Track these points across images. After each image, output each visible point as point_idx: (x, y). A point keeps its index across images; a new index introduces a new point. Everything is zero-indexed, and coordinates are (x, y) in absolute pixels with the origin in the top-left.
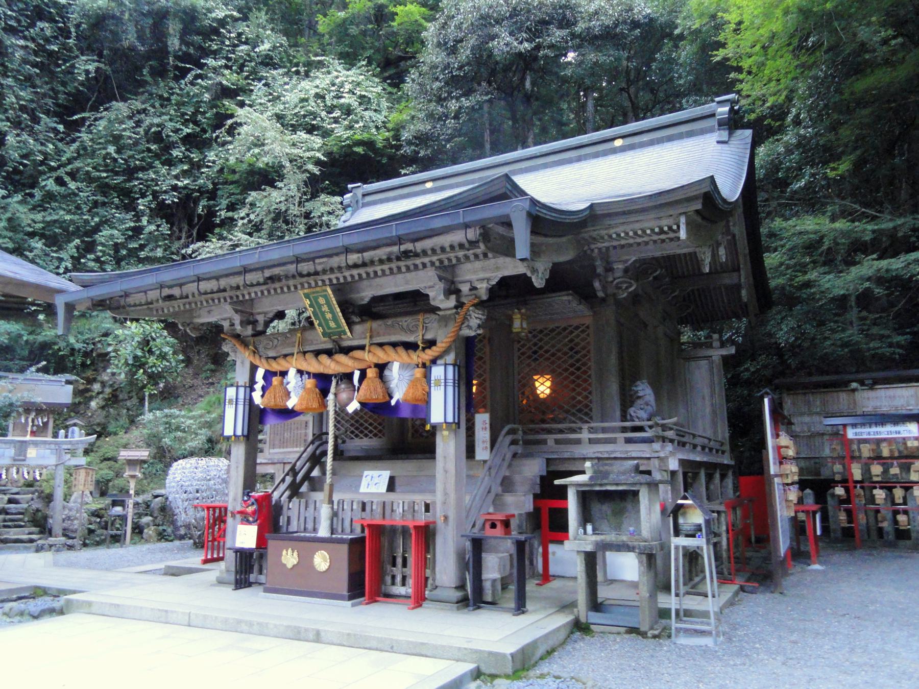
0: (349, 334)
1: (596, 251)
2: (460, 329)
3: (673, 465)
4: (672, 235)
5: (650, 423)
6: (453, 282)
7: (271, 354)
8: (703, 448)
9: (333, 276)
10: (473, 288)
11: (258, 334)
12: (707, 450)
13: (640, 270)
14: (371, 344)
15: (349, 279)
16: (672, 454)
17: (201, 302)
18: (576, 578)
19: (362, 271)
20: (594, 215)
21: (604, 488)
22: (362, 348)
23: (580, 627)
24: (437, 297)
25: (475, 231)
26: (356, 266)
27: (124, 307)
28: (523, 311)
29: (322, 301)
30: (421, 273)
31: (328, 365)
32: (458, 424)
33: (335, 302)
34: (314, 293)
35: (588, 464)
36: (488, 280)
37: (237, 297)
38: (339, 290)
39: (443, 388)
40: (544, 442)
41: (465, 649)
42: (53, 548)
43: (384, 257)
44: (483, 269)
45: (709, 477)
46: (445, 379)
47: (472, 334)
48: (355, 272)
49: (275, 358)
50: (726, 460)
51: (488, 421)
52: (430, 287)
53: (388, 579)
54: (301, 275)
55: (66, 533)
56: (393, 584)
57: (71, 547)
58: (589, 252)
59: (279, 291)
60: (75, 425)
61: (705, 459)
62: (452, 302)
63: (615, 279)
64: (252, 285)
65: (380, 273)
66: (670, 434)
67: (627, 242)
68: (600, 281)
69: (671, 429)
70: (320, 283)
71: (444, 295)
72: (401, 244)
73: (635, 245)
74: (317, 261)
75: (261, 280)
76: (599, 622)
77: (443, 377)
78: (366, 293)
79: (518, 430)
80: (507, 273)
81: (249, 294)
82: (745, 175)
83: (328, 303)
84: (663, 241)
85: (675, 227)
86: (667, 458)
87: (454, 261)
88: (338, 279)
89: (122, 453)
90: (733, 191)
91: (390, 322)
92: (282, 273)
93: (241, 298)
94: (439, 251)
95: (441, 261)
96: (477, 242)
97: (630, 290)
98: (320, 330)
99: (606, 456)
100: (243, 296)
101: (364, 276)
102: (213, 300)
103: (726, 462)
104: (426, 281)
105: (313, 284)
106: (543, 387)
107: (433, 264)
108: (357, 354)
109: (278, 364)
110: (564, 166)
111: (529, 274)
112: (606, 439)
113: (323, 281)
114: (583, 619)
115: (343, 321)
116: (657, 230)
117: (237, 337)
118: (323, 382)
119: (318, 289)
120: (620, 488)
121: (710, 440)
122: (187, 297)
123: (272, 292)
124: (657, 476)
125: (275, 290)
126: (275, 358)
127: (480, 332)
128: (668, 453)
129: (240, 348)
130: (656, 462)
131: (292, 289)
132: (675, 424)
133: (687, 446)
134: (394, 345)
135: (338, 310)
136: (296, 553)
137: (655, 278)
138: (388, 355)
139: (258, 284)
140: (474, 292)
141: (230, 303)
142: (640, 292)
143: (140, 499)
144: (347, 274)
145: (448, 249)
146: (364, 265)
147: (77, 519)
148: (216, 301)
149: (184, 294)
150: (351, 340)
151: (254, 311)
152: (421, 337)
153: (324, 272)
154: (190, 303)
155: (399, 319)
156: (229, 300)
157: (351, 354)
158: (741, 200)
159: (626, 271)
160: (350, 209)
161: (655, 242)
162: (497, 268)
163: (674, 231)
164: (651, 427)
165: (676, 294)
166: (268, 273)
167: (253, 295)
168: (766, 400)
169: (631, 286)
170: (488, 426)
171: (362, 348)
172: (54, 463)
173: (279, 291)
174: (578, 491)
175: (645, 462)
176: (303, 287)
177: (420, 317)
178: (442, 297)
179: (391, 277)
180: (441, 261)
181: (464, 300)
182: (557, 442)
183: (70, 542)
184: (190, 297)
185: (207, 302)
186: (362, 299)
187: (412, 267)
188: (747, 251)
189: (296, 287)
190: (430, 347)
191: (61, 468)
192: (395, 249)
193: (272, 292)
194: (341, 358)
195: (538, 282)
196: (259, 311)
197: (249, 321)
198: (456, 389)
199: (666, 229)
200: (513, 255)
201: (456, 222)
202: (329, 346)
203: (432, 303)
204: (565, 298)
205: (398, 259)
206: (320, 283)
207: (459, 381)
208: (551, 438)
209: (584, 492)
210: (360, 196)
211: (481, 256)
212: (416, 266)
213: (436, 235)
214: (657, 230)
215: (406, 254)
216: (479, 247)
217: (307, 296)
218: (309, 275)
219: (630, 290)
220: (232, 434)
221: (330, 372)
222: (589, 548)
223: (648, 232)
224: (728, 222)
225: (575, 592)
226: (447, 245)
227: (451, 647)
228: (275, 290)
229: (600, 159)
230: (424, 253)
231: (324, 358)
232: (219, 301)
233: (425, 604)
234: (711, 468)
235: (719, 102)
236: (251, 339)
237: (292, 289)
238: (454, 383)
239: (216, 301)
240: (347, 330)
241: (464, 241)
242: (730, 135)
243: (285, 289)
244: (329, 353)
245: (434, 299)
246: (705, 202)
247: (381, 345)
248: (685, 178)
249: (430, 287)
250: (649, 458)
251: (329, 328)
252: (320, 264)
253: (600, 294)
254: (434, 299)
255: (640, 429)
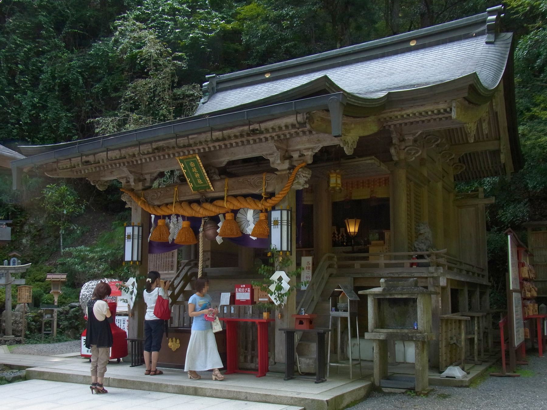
0: (212, 188)
1: (392, 127)
2: (292, 184)
3: (443, 282)
4: (447, 115)
5: (427, 253)
6: (287, 151)
7: (157, 203)
8: (468, 272)
9: (200, 147)
10: (302, 155)
11: (146, 189)
12: (471, 274)
13: (425, 139)
14: (228, 196)
15: (212, 149)
16: (443, 274)
17: (107, 166)
18: (372, 361)
19: (221, 143)
20: (394, 100)
21: (393, 297)
22: (222, 198)
23: (373, 391)
24: (276, 162)
25: (303, 115)
26: (218, 140)
27: (56, 170)
28: (338, 171)
29: (192, 164)
30: (264, 144)
31: (200, 212)
32: (291, 252)
33: (201, 165)
34: (187, 159)
35: (382, 280)
36: (312, 149)
37: (133, 162)
38: (204, 156)
39: (279, 226)
40: (352, 266)
41: (296, 398)
42: (7, 343)
43: (238, 134)
44: (309, 141)
45: (471, 294)
46: (281, 220)
47: (301, 188)
48: (217, 144)
49: (159, 206)
50: (485, 282)
51: (311, 262)
52: (270, 155)
53: (242, 358)
54: (180, 147)
55: (15, 333)
56: (246, 361)
57: (19, 342)
58: (387, 128)
59: (162, 157)
60: (14, 256)
61: (468, 280)
62: (286, 165)
63: (406, 147)
64: (144, 154)
65: (234, 144)
66: (442, 261)
67: (415, 120)
68: (395, 148)
69: (442, 257)
70: (191, 152)
71: (281, 160)
72: (250, 125)
73: (420, 123)
74: (190, 137)
75: (150, 150)
76: (387, 386)
77: (279, 219)
78: (224, 159)
79: (334, 257)
80: (326, 144)
81: (141, 160)
82: (504, 68)
83: (197, 166)
84: (440, 119)
85: (448, 110)
86: (439, 277)
87: (288, 136)
88: (204, 149)
89: (48, 276)
90: (494, 81)
91: (241, 179)
92: (165, 145)
93: (135, 163)
94: (277, 130)
95: (279, 137)
96: (305, 123)
97: (417, 155)
98: (191, 185)
99: (396, 276)
100: (137, 161)
101: (223, 146)
102: (115, 164)
103: (484, 283)
104: (267, 149)
105: (187, 153)
106: (353, 229)
107: (272, 138)
108: (219, 203)
109: (162, 210)
110: (372, 61)
111: (342, 145)
112: (396, 263)
113: (194, 150)
114: (377, 383)
115: (208, 179)
116: (435, 112)
117: (132, 190)
118: (194, 223)
119: (190, 156)
120: (404, 297)
121: (473, 266)
122: (99, 162)
123: (157, 158)
124: (431, 289)
125: (159, 157)
126: (159, 206)
127: (307, 186)
128: (439, 274)
129: (134, 199)
130: (431, 280)
131: (172, 156)
132: (445, 254)
133: (455, 270)
134: (245, 196)
135: (204, 171)
136: (178, 340)
137: (437, 145)
138: (241, 203)
139: (148, 153)
140: (302, 158)
141: (127, 167)
142: (425, 156)
143: (60, 309)
144: (211, 145)
145: (284, 128)
146: (224, 139)
147: (20, 323)
148: (118, 165)
149: (97, 161)
150: (213, 192)
151: (143, 172)
152: (264, 190)
153: (196, 144)
154: (99, 167)
155: (248, 177)
156: (126, 164)
157: (215, 202)
158: (502, 88)
159: (415, 141)
160: (207, 94)
161: (435, 119)
162: (318, 140)
163: (448, 112)
164: (429, 256)
165: (453, 157)
166: (155, 145)
167: (144, 161)
168: (509, 236)
169: (417, 152)
170: (311, 266)
171: (222, 198)
172: (5, 283)
173: (162, 157)
174: (375, 299)
175: (424, 280)
176: (179, 156)
177: (264, 176)
178: (279, 161)
179: (242, 147)
180: (279, 137)
181: (295, 163)
182: (362, 266)
183: (17, 339)
184: (101, 162)
185: (111, 165)
186: (221, 163)
187: (258, 140)
188: (506, 124)
189: (174, 155)
190: (270, 198)
191: (9, 286)
192: (246, 128)
193: (157, 158)
194: (208, 206)
195: (348, 151)
196: (147, 172)
197: (140, 179)
198: (289, 227)
199: (442, 111)
200: (330, 133)
201: (290, 110)
202: (197, 197)
203: (272, 166)
204: (370, 161)
205: (248, 135)
206: (191, 152)
207: (291, 221)
208: (357, 264)
209: (379, 300)
210: (215, 84)
211: (308, 133)
212: (261, 140)
213: (275, 119)
214: (435, 112)
215: (254, 132)
216: (306, 127)
217: (182, 161)
218: (184, 146)
219: (417, 155)
220: (130, 259)
221: (200, 216)
222: (382, 337)
223: (430, 113)
224: (492, 103)
225: (373, 369)
226: (283, 125)
227: (287, 397)
228: (159, 157)
229: (399, 55)
230: (267, 130)
231: (195, 206)
232: (120, 165)
233: (267, 374)
234: (472, 286)
235: (489, 12)
236: (143, 193)
237: (172, 156)
238: (288, 223)
239: (118, 165)
240: (211, 186)
241: (295, 122)
242: (496, 38)
243: (167, 157)
244: (198, 202)
245: (273, 163)
246: (468, 89)
247: (235, 196)
248: (460, 71)
249: (270, 155)
250: (427, 278)
251: (197, 183)
252: (192, 139)
253: (395, 158)
254: (273, 163)
255: (421, 257)
